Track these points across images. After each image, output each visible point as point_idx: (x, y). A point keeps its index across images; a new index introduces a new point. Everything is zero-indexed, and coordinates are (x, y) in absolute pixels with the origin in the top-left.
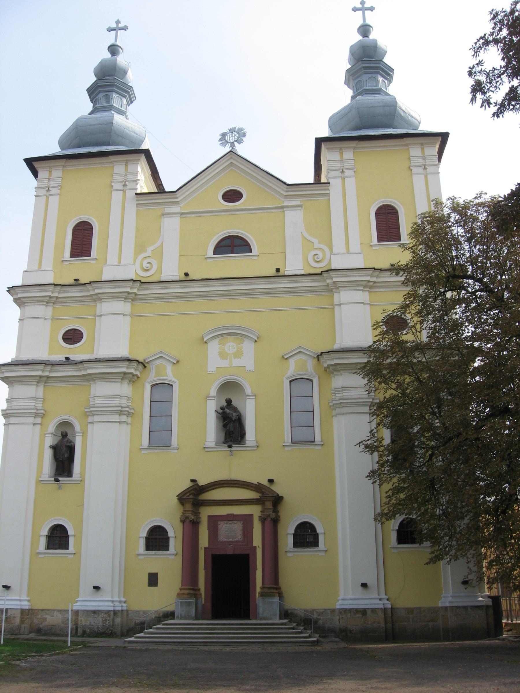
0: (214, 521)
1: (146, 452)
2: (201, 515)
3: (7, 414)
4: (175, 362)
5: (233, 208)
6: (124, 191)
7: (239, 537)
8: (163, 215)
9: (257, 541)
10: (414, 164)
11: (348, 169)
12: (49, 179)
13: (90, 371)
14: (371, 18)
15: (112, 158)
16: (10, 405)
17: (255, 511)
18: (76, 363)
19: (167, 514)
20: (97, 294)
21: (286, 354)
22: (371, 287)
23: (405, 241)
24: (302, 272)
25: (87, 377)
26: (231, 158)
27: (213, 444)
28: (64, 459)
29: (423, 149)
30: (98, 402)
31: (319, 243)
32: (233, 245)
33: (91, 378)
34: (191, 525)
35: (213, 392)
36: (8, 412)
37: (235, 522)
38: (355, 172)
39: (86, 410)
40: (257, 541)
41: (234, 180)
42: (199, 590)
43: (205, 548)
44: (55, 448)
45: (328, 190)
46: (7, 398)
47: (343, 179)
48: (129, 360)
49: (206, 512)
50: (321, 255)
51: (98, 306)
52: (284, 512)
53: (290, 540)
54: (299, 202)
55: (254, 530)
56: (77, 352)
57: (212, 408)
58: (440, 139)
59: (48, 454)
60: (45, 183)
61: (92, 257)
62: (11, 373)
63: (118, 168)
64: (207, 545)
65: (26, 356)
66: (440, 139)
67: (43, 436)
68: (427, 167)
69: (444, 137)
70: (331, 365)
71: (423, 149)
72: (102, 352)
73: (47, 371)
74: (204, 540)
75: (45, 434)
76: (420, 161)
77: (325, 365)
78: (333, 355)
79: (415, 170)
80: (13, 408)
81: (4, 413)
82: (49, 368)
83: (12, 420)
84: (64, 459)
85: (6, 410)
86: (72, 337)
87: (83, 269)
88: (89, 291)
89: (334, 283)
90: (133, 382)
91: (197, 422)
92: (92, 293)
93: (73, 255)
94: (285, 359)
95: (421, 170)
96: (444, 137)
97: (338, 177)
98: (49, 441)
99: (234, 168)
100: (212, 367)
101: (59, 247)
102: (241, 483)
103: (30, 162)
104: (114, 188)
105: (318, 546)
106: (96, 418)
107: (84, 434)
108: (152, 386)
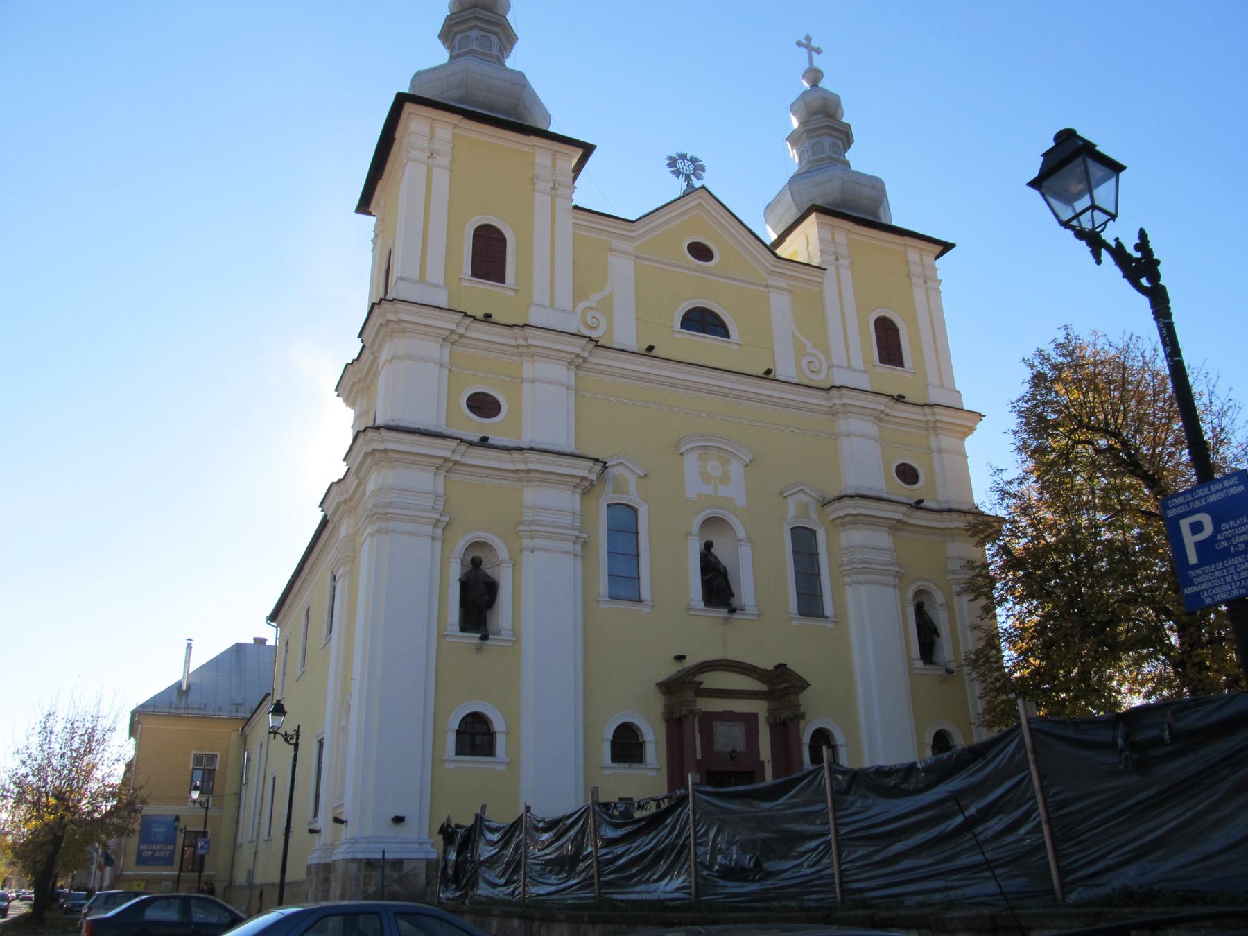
7: (741, 747)
9: (765, 753)
14: (818, 62)
17: (759, 708)
22: (881, 420)
28: (478, 599)
32: (702, 321)
33: (528, 475)
34: (675, 724)
35: (695, 528)
40: (765, 753)
41: (696, 230)
44: (465, 585)
55: (760, 736)
58: (580, 152)
66: (580, 152)
69: (588, 149)
77: (832, 517)
78: (847, 501)
84: (478, 599)
91: (671, 571)
96: (588, 149)
106: (538, 542)
107: (516, 564)
108: (609, 506)
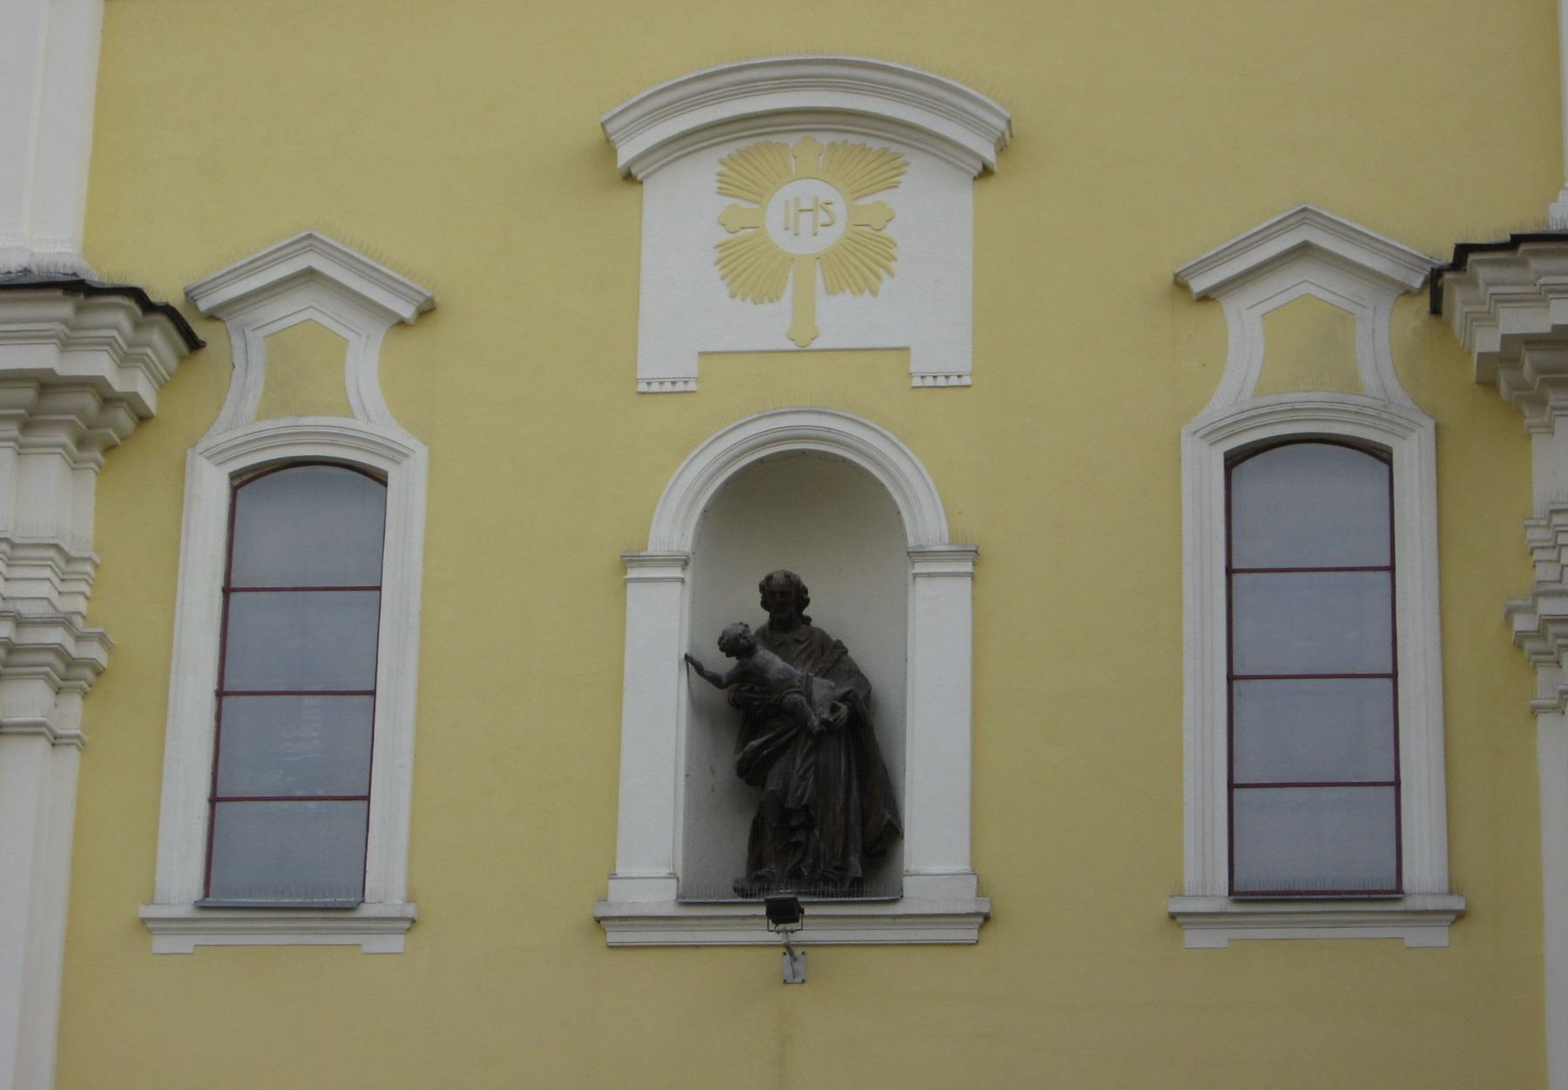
4: (407, 312)
27: (660, 897)
35: (673, 527)
48: (75, 287)
57: (660, 640)
70: (1533, 341)
90: (109, 448)
94: (1194, 295)
100: (665, 353)
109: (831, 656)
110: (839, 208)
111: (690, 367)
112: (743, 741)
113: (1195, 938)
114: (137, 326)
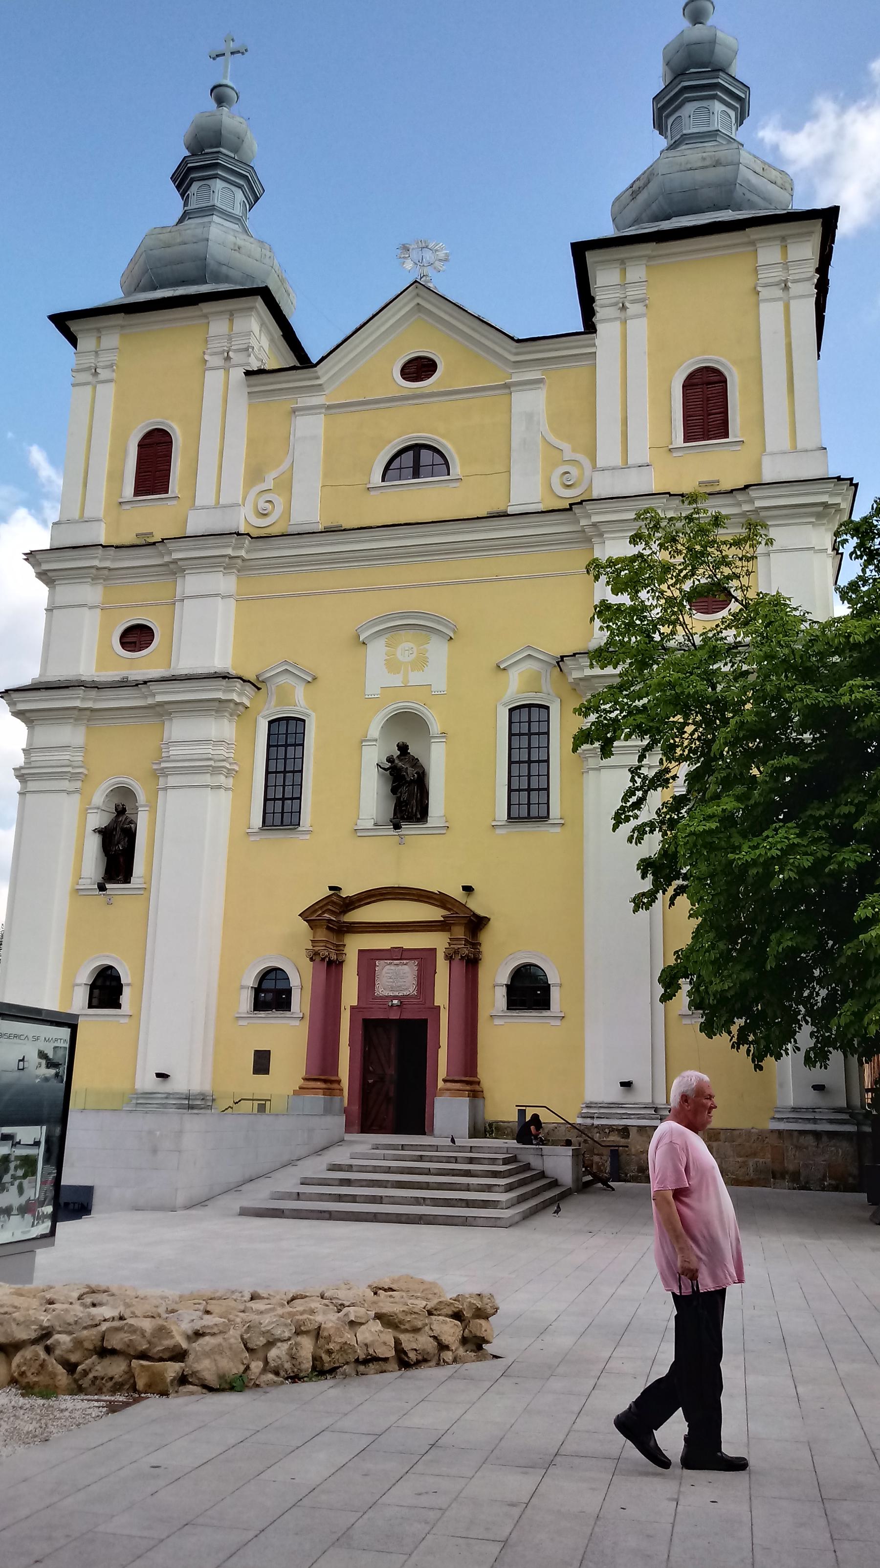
0: (368, 958)
1: (257, 838)
2: (346, 950)
3: (23, 775)
4: (310, 679)
5: (418, 392)
6: (227, 370)
8: (294, 411)
9: (441, 997)
10: (766, 281)
11: (633, 302)
12: (96, 352)
13: (159, 698)
15: (206, 308)
16: (28, 761)
17: (438, 941)
18: (137, 685)
19: (287, 946)
20: (175, 562)
21: (505, 660)
23: (736, 436)
24: (541, 507)
25: (158, 709)
26: (418, 295)
27: (370, 824)
28: (118, 850)
29: (785, 248)
30: (174, 751)
31: (574, 450)
32: (416, 460)
35: (375, 731)
36: (23, 771)
37: (405, 962)
38: (646, 306)
39: (155, 767)
42: (339, 1082)
43: (352, 1008)
45: (594, 345)
46: (24, 747)
47: (624, 322)
48: (226, 677)
49: (355, 944)
50: (574, 471)
51: (179, 581)
52: (489, 941)
53: (501, 996)
54: (539, 372)
56: (143, 664)
57: (373, 756)
59: (93, 844)
60: (90, 360)
61: (170, 494)
62: (34, 700)
63: (218, 324)
64: (355, 1003)
65: (56, 674)
67: (85, 812)
68: (789, 284)
70: (581, 679)
71: (785, 248)
72: (185, 665)
73: (90, 699)
74: (350, 995)
75: (87, 809)
76: (777, 274)
79: (764, 293)
80: (33, 765)
81: (18, 773)
82: (93, 693)
83: (32, 786)
84: (118, 850)
85: (21, 768)
86: (137, 637)
87: (155, 517)
88: (162, 555)
89: (594, 525)
90: (239, 716)
91: (345, 783)
92: (167, 559)
93: (137, 493)
94: (500, 669)
95: (778, 292)
97: (616, 319)
98: (98, 820)
99: (423, 316)
100: (373, 688)
101: (115, 477)
102: (414, 892)
103: (63, 322)
104: (208, 365)
105: (549, 1009)
106: (172, 781)
109: (415, 762)
110: (415, 649)
111: (379, 691)
112: (394, 782)
113: (499, 831)
114: (242, 685)
